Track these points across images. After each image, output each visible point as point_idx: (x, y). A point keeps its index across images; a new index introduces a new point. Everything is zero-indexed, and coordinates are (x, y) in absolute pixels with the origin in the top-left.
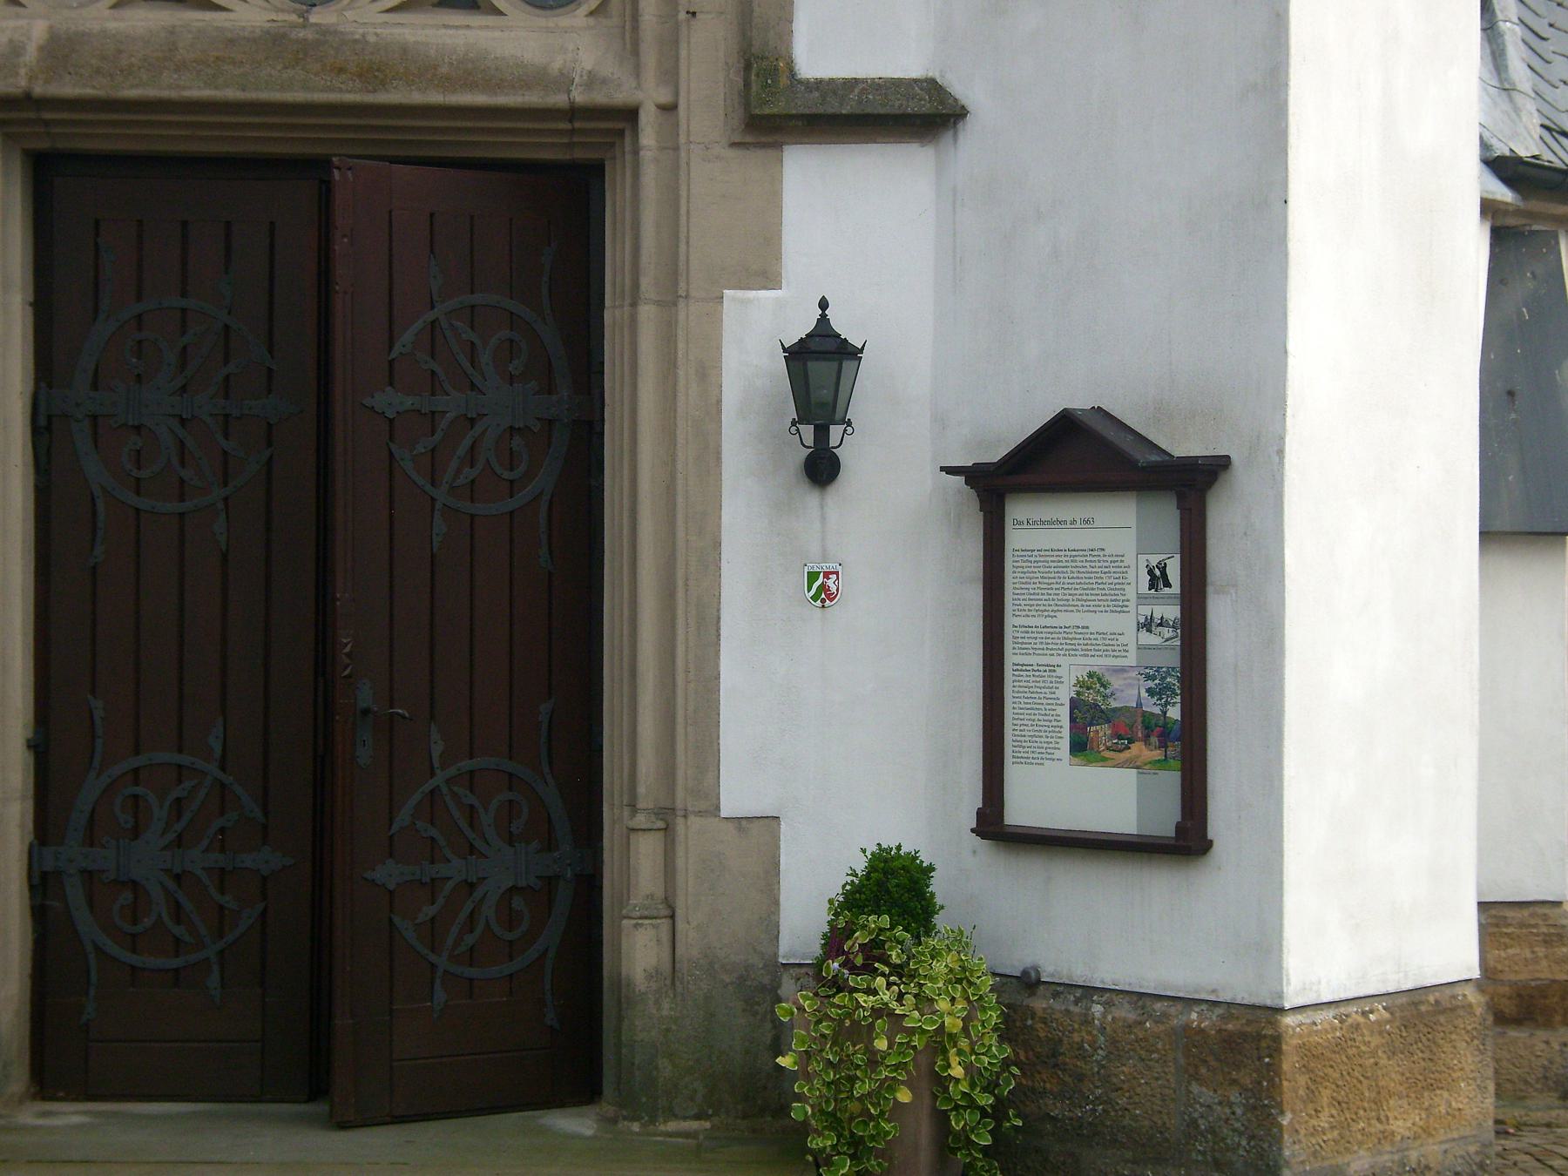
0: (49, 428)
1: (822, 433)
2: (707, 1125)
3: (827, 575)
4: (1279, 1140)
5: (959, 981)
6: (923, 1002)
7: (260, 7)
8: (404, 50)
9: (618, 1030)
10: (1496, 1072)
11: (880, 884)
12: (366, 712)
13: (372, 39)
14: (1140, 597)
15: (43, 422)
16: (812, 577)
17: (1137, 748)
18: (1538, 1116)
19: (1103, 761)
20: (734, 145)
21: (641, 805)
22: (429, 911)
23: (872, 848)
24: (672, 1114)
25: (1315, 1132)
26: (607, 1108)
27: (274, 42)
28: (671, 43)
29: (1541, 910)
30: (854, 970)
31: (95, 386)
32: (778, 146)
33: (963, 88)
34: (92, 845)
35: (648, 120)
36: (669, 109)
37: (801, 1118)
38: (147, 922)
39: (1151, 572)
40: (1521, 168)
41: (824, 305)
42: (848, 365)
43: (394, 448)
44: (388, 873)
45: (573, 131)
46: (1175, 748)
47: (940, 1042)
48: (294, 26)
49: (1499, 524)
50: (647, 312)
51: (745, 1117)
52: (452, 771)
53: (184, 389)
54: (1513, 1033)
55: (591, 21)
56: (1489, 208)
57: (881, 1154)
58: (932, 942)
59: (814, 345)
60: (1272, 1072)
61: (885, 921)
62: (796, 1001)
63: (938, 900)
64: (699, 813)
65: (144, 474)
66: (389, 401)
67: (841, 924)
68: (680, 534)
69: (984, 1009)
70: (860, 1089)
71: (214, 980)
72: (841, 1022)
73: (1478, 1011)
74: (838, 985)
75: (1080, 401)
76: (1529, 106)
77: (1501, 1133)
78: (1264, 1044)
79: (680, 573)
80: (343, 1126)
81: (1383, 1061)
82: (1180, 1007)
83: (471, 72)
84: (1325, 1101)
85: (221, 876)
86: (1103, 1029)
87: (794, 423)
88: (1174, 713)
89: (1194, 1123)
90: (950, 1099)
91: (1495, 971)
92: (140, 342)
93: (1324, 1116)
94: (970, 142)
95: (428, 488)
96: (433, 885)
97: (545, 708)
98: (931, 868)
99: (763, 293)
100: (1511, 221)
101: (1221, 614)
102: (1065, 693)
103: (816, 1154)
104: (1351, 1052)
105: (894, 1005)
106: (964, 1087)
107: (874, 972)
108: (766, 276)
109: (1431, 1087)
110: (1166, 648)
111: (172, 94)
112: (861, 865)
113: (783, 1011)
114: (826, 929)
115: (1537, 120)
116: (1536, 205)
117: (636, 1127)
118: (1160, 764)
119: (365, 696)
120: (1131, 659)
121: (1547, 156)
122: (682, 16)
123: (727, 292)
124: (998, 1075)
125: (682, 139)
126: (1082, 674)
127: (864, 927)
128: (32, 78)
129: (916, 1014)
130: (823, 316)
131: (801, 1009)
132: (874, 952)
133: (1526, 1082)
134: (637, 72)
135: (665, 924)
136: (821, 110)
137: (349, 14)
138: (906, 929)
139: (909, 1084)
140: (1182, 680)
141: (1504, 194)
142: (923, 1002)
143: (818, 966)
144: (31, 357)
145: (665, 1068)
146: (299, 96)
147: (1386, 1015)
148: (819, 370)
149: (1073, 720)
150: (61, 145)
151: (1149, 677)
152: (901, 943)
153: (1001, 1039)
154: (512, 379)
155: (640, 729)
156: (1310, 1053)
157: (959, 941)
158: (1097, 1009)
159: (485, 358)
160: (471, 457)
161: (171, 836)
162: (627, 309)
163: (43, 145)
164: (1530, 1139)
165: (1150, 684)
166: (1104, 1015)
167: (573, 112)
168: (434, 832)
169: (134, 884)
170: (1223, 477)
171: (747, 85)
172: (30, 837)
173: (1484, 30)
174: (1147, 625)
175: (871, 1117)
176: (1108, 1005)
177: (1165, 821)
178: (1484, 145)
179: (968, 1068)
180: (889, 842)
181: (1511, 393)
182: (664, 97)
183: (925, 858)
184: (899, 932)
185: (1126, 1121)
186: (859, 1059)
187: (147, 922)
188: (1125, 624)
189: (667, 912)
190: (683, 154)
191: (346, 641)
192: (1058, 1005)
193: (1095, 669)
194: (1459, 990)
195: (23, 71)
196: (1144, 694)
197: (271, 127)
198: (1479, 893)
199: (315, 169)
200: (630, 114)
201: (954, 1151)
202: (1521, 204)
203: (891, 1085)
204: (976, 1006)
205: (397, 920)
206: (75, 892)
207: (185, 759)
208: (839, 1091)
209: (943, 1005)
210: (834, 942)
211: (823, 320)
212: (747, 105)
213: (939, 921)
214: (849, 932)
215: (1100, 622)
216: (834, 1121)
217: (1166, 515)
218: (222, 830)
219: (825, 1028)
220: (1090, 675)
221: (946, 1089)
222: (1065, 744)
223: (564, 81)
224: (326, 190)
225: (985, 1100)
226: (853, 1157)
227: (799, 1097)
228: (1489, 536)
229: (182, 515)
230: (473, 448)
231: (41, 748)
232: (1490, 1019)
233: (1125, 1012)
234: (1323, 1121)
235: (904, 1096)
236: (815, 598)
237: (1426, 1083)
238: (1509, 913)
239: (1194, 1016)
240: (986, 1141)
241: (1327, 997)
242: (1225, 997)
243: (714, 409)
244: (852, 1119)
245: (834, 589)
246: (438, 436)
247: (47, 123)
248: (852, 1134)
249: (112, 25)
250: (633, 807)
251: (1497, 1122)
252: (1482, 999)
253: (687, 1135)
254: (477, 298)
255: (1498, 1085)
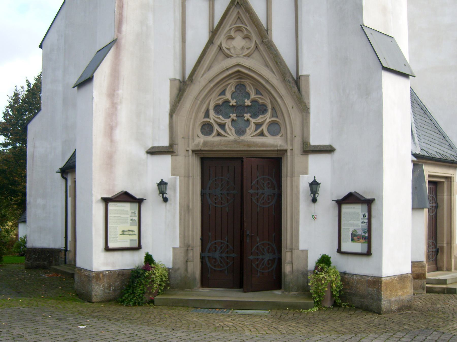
0: (203, 195)
1: (314, 195)
2: (297, 293)
3: (315, 215)
4: (381, 296)
5: (335, 273)
6: (329, 276)
7: (213, 116)
8: (253, 142)
9: (284, 279)
10: (413, 286)
11: (323, 259)
12: (248, 235)
13: (249, 141)
14: (362, 219)
15: (202, 194)
16: (313, 216)
17: (361, 240)
18: (420, 292)
19: (356, 242)
20: (301, 155)
21: (288, 248)
22: (257, 263)
23: (322, 254)
24: (292, 291)
25: (387, 295)
26: (282, 290)
27: (235, 141)
28: (292, 141)
29: (420, 263)
30: (319, 272)
31: (210, 189)
32: (308, 155)
33: (334, 146)
34: (209, 253)
35: (289, 151)
36: (292, 150)
37: (311, 292)
38: (217, 264)
39: (363, 215)
40: (417, 155)
41: (315, 177)
42: (318, 186)
43: (252, 198)
44: (251, 257)
45: (278, 153)
46: (367, 240)
47: (332, 282)
48: (238, 139)
49: (415, 207)
50: (289, 178)
51: (303, 292)
52: (260, 243)
53: (222, 190)
54: (416, 280)
55: (280, 137)
56: (413, 161)
57: (323, 297)
58: (331, 268)
59: (313, 183)
60: (381, 286)
61: (324, 265)
62: (311, 276)
63: (331, 262)
64: (296, 249)
65: (216, 201)
66: (251, 191)
67: (317, 265)
68: (294, 209)
69: (338, 277)
70: (320, 288)
71: (226, 272)
72: (317, 278)
73: (411, 277)
74: (317, 274)
75: (352, 191)
76: (418, 146)
77: (414, 295)
78: (379, 282)
79: (294, 215)
80: (245, 292)
81: (397, 285)
82: (367, 277)
83: (263, 145)
84: (388, 290)
85: (227, 258)
86: (355, 280)
87: (310, 194)
88: (367, 235)
89: (369, 293)
90: (333, 290)
91: (413, 271)
92: (216, 183)
93: (388, 292)
94: (336, 155)
95: (257, 203)
96: (258, 259)
97: (274, 234)
98: (330, 257)
99: (306, 175)
100: (416, 163)
101: (373, 221)
102: (350, 232)
103: (313, 297)
104: (392, 283)
105: (325, 276)
106: (335, 288)
107: (322, 272)
108: (306, 173)
109: (404, 288)
110: (365, 226)
111: (221, 149)
112: (320, 257)
113: (309, 277)
114: (315, 266)
115: (419, 148)
116: (420, 160)
117: (287, 293)
118: (365, 242)
119: (248, 233)
120: (360, 227)
121: (421, 153)
122: (294, 137)
123: (300, 175)
124: (340, 286)
125: (294, 154)
126: (353, 230)
127: (321, 266)
128: (201, 147)
129: (328, 278)
130: (315, 179)
131: (312, 277)
132: (322, 269)
133: (418, 288)
134: (287, 144)
135: (291, 265)
136: (314, 150)
137: (246, 137)
138: (327, 266)
139: (327, 288)
140: (368, 230)
141: (415, 159)
142: (329, 276)
143: (314, 271)
144: (201, 185)
145: (291, 285)
146: (239, 149)
147: (397, 278)
148: (314, 186)
149: (351, 236)
150: (205, 156)
151: (363, 230)
152: (326, 268)
153: (341, 281)
154: (269, 188)
155: (288, 238)
156: (386, 283)
157: (334, 267)
158: (355, 277)
159: (265, 185)
160: (263, 199)
161: (220, 252)
162: (286, 178)
163: (202, 156)
164: (418, 296)
165: (363, 231)
166: (356, 278)
167: (278, 150)
168: (258, 252)
169: (215, 258)
170: (374, 202)
171: (303, 146)
172: (200, 251)
173: (411, 135)
174: (363, 223)
175: (321, 292)
176: (356, 277)
177: (365, 250)
178: (412, 152)
179: (336, 285)
180: (324, 253)
181: (416, 188)
182: (291, 148)
183: (330, 256)
184: (326, 266)
185: (359, 293)
186: (320, 284)
187: (217, 264)
188: (359, 222)
189: (291, 263)
190: (294, 156)
191: (245, 225)
192: (349, 277)
193: (355, 229)
194: (408, 274)
195: (200, 146)
196: (362, 233)
197: (235, 153)
198: (411, 260)
199: (241, 159)
200: (286, 151)
201: (334, 297)
202: (417, 160)
203: (325, 288)
204: (337, 277)
205: (253, 264)
206: (207, 259)
207: (222, 241)
208: (317, 289)
209: (332, 276)
210: (316, 268)
211: (315, 179)
212: (303, 149)
213: (332, 265)
214: (318, 266)
215: (356, 222)
216: (316, 293)
217: (365, 207)
218: (227, 251)
219: (315, 280)
220: (354, 230)
221: (332, 288)
222: (350, 239)
223: (277, 146)
224: (242, 162)
225: (338, 290)
226: (319, 297)
227: (311, 289)
228: (413, 208)
229: (222, 207)
230: (263, 198)
231: (202, 240)
232: (413, 278)
233: (359, 278)
234: (388, 293)
235: (326, 289)
236: (313, 219)
237: (403, 287)
238: (415, 263)
239: (369, 278)
240: (338, 296)
241: (389, 275)
242: (374, 275)
243: (298, 192)
244: (319, 292)
245: (316, 217)
246: (258, 196)
247: (203, 153)
248: (319, 294)
249: (212, 140)
250: (287, 248)
251: (414, 293)
252: (412, 276)
253: (295, 294)
254: (264, 177)
255: (414, 288)
